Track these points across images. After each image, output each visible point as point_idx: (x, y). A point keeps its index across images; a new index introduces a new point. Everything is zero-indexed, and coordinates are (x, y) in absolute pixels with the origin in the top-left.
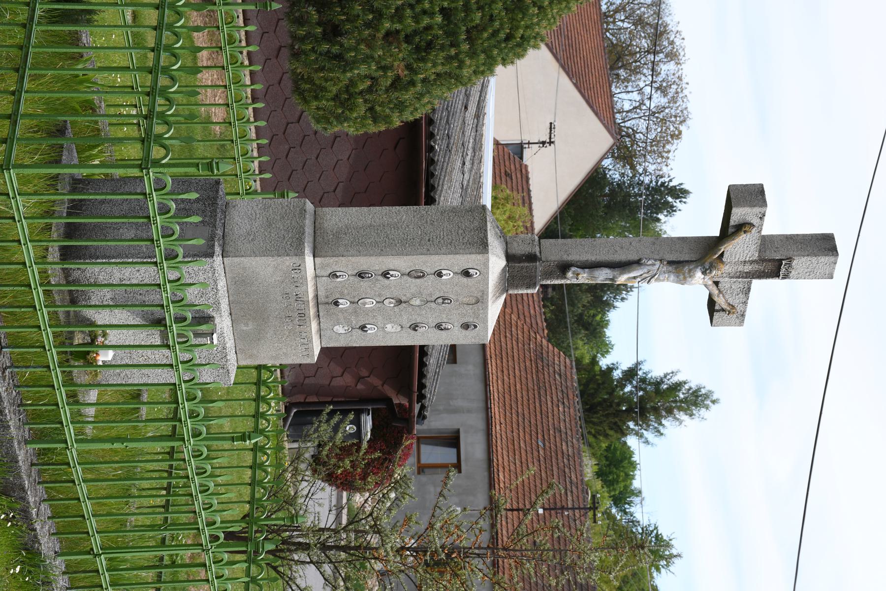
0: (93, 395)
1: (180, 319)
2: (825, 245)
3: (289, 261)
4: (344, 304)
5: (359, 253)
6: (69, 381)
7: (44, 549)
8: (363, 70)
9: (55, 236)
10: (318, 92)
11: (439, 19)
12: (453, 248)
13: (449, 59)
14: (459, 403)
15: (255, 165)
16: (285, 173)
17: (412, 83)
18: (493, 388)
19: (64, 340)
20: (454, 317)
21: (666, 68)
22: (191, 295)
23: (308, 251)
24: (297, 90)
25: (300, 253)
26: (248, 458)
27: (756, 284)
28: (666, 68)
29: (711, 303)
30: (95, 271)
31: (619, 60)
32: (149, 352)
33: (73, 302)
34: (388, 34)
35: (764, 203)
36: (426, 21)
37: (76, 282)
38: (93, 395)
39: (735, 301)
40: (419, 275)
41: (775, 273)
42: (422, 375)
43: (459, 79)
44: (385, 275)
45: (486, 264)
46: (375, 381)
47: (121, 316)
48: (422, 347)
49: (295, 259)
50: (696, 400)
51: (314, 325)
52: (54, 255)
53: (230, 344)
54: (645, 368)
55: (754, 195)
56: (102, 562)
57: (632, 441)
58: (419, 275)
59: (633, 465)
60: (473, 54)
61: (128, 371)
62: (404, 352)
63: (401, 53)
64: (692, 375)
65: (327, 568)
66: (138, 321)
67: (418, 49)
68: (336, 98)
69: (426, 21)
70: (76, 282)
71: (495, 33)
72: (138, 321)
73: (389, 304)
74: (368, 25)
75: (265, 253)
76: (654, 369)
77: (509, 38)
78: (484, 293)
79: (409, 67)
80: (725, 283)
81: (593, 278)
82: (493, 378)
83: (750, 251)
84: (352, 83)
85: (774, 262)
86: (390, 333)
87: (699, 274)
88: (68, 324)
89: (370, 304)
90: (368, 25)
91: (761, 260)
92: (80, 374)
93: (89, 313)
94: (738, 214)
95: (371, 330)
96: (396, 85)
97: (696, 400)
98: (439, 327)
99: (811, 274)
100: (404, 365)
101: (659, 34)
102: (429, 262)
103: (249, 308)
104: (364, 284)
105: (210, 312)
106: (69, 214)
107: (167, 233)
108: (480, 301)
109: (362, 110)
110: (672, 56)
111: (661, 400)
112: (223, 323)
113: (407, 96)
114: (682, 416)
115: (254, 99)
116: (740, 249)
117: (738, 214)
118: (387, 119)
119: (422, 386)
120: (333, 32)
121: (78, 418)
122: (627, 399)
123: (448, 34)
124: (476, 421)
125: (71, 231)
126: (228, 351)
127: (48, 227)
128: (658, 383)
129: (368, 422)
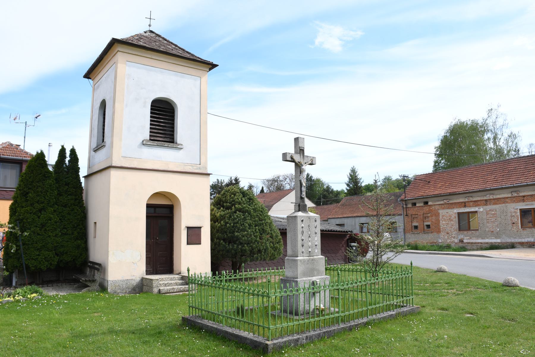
0: (332, 309)
1: (313, 289)
2: (296, 140)
3: (299, 263)
4: (310, 250)
5: (297, 246)
6: (328, 314)
7: (366, 321)
8: (268, 245)
9: (292, 317)
10: (273, 255)
11: (257, 227)
12: (296, 224)
13: (266, 225)
14: (353, 223)
15: (281, 270)
16: (281, 264)
17: (271, 233)
18: (350, 215)
19: (318, 316)
20: (314, 224)
21: (281, 178)
22: (307, 286)
23: (297, 258)
24: (273, 260)
25: (297, 260)
26: (343, 272)
27: (305, 154)
28: (281, 178)
29: (310, 164)
30: (301, 308)
31: (279, 188)
32: (321, 296)
33: (309, 313)
34: (260, 239)
35: (286, 153)
36: (257, 230)
37: (304, 312)
38: (332, 309)
39: (310, 159)
40: (303, 232)
41: (303, 150)
42: (342, 232)
43: (271, 223)
44: (303, 240)
45: (300, 216)
46: (343, 242)
47: (312, 302)
48: (321, 231)
49: (298, 261)
50: (353, 171)
51: (315, 257)
52: (297, 317)
53: (320, 277)
54: (346, 182)
55: (284, 155)
56: (370, 307)
57: (363, 185)
58: (303, 232)
59: (369, 184)
60: (265, 220)
61: (326, 301)
62: (322, 235)
63: (265, 236)
64: (348, 172)
65: (383, 253)
66: (314, 298)
67: (263, 232)
68: (274, 251)
69: (257, 230)
70: (304, 312)
71: (261, 215)
72: (314, 298)
73: (310, 239)
74: (258, 243)
75: (297, 268)
76: (347, 180)
77: (262, 212)
78: (307, 217)
79: (268, 234)
80: (305, 161)
81: (184, 229)
82: (348, 216)
83: (298, 156)
84: (271, 247)
85: (301, 151)
86: (317, 239)
87: (303, 167)
88: (314, 315)
89: (310, 244)
90: (258, 243)
91: (300, 153)
92: (327, 311)
93: (311, 310)
94: (289, 159)
95: (316, 243)
96: (271, 237)
97: (353, 171)
98: (316, 227)
99: (303, 142)
100: (325, 235)
101: (274, 181)
102: (300, 230)
103: (311, 272)
104: (305, 245)
105: (311, 282)
106: (287, 313)
107: (291, 291)
108: (309, 218)
109: (277, 245)
110: (278, 177)
111: (354, 179)
112: (314, 279)
113: (274, 235)
114: (357, 174)
115: (278, 269)
116: (297, 158)
117: (289, 159)
118: (280, 239)
119: (344, 232)
120: (259, 251)
121: (338, 312)
122: (354, 186)
123: (260, 225)
124: (357, 219)
125: (291, 313)
126: (321, 278)
127: (290, 319)
128: (350, 179)
129: (353, 244)
